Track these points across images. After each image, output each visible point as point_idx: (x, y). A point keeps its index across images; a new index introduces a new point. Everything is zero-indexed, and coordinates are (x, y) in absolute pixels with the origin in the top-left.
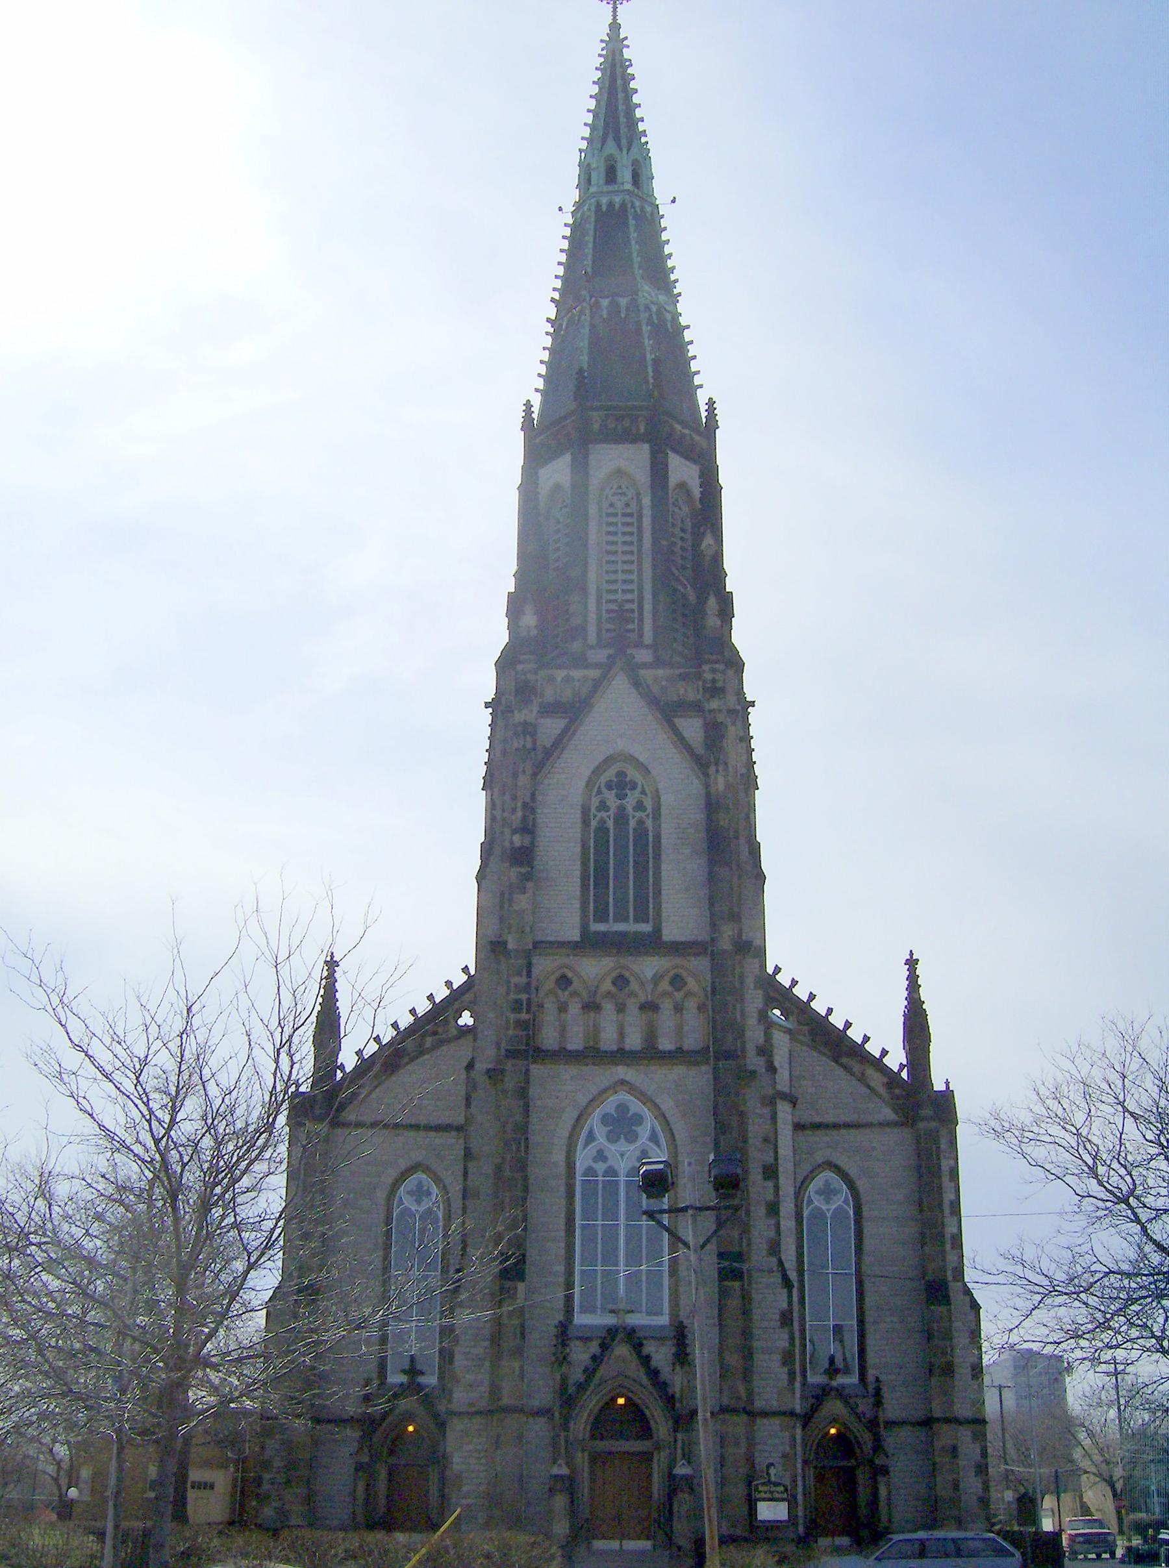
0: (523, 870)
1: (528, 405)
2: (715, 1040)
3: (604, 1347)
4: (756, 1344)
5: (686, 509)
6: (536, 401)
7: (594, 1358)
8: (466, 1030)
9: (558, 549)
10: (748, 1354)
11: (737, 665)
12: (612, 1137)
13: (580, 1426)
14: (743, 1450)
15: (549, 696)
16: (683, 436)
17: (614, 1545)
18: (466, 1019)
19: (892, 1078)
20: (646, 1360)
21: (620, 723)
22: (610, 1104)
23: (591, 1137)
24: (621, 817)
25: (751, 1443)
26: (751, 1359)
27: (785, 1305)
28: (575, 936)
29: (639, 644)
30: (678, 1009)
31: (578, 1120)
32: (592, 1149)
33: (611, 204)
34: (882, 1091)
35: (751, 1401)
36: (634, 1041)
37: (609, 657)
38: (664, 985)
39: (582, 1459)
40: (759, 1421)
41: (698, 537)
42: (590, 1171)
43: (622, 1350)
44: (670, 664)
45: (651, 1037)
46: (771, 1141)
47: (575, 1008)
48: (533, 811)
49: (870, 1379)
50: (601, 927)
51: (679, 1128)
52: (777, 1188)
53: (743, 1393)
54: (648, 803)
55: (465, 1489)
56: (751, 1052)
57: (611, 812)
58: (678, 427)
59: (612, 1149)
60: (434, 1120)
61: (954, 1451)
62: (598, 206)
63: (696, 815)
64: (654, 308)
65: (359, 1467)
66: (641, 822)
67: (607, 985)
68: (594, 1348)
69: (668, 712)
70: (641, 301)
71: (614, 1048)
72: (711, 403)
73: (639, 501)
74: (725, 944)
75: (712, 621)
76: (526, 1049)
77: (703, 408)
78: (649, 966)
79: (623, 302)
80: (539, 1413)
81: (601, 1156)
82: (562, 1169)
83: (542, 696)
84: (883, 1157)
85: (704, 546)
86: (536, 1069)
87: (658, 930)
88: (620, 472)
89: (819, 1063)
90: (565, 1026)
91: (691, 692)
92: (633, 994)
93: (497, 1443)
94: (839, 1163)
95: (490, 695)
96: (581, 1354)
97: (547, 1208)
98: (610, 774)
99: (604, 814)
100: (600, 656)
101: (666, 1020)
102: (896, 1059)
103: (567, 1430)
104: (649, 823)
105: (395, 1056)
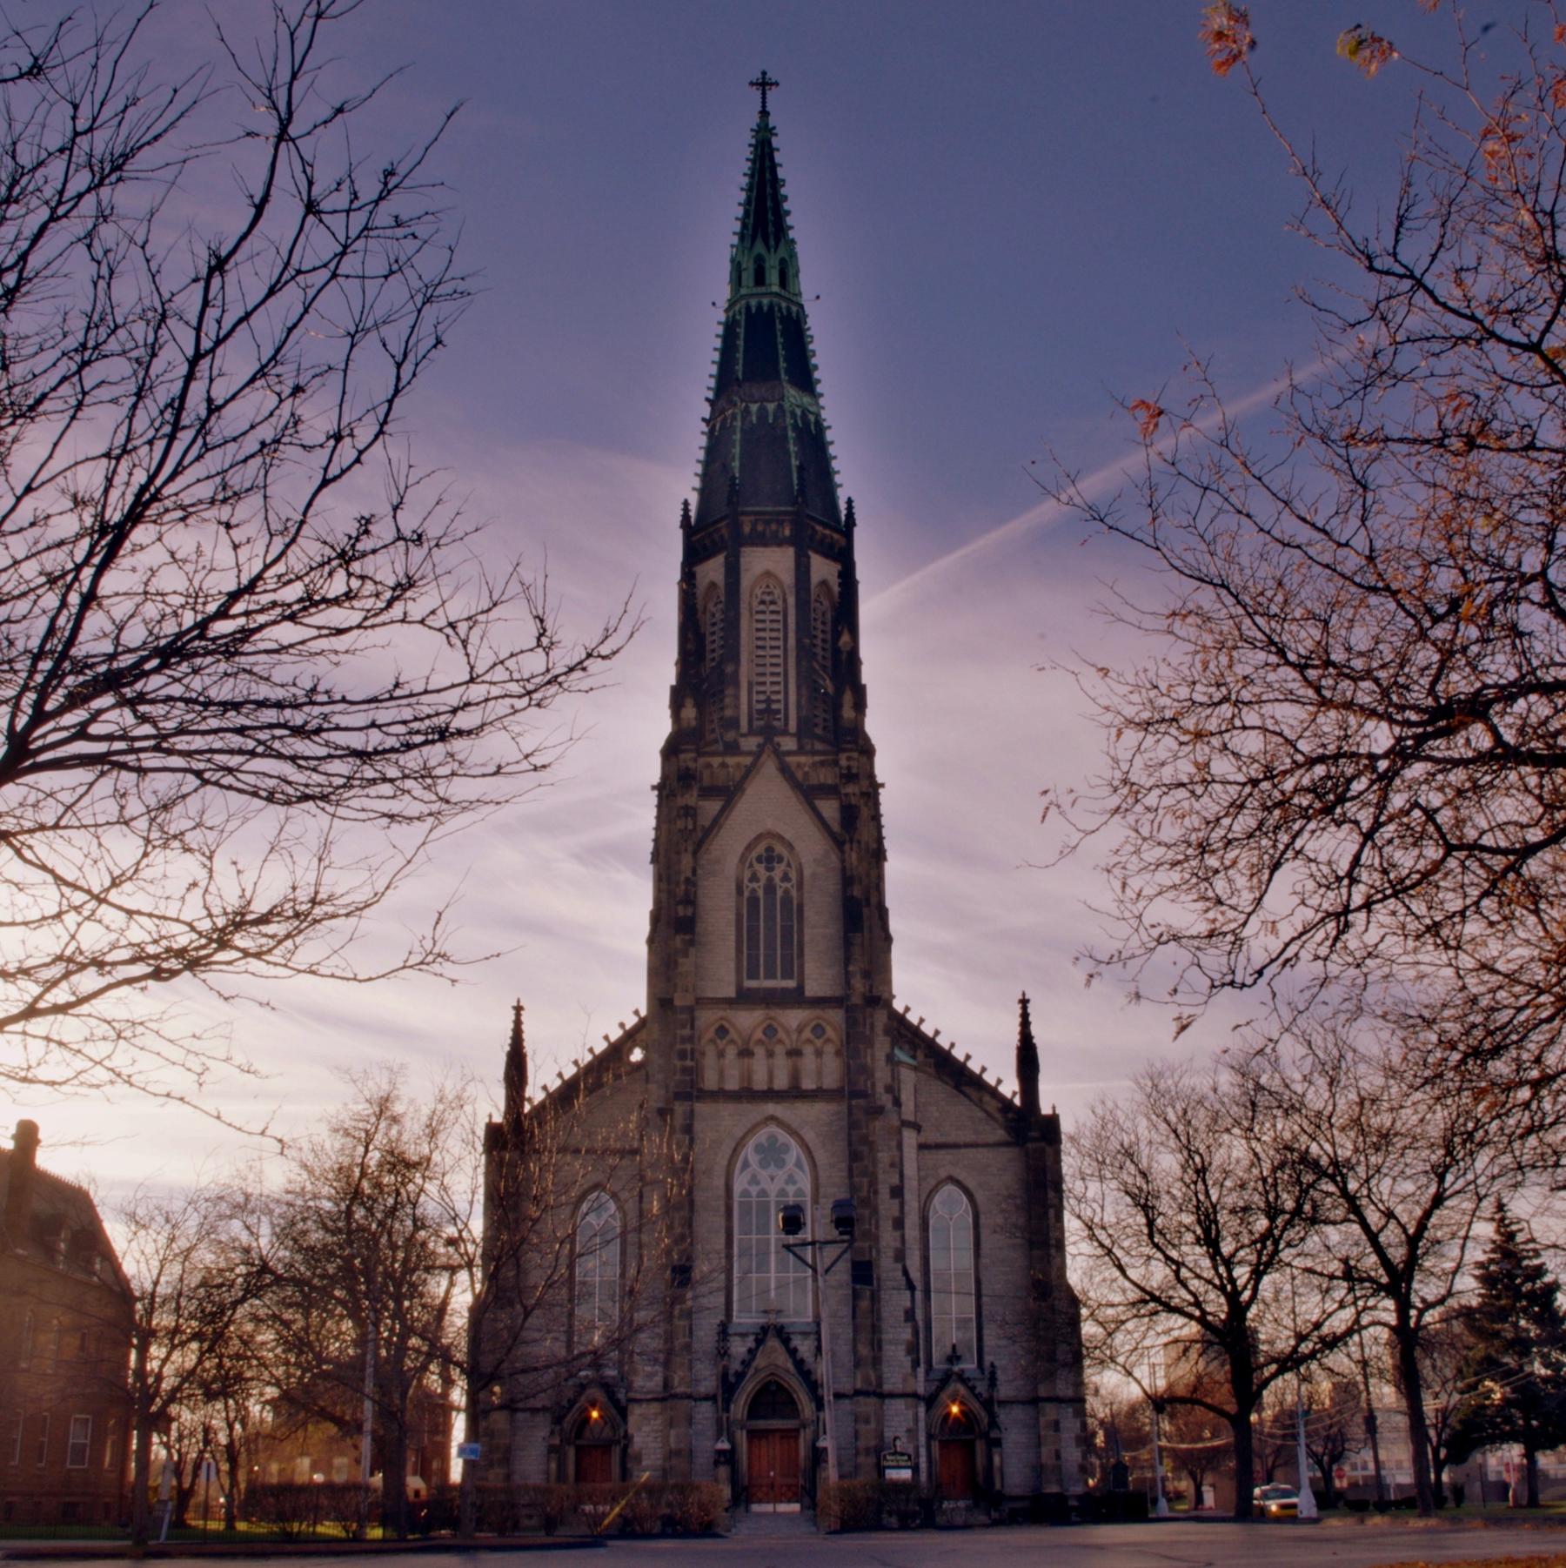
0: (687, 937)
1: (686, 503)
2: (850, 1082)
3: (759, 1341)
4: (884, 1336)
5: (826, 603)
6: (694, 499)
7: (750, 1351)
8: (639, 1066)
9: (714, 624)
10: (876, 1345)
11: (868, 751)
12: (764, 1164)
13: (739, 1408)
14: (873, 1425)
15: (706, 781)
16: (825, 536)
17: (769, 1508)
18: (637, 1055)
19: (1006, 1104)
20: (793, 1352)
21: (768, 807)
22: (762, 1136)
23: (746, 1165)
24: (770, 888)
25: (880, 1420)
26: (880, 1348)
27: (908, 1304)
28: (731, 992)
29: (785, 732)
30: (819, 1053)
31: (735, 1150)
32: (746, 1176)
33: (760, 306)
34: (998, 1115)
35: (880, 1384)
36: (781, 1082)
37: (759, 746)
38: (807, 1034)
39: (742, 1437)
40: (887, 1401)
41: (837, 635)
42: (746, 1193)
43: (773, 1343)
44: (814, 753)
45: (795, 1076)
46: (898, 1165)
47: (731, 1052)
48: (695, 885)
49: (987, 1364)
50: (752, 984)
51: (821, 1157)
52: (902, 1205)
53: (873, 1378)
54: (793, 875)
55: (644, 1463)
56: (880, 1089)
57: (762, 883)
58: (819, 528)
59: (764, 1174)
60: (315, 503)
61: (1056, 1426)
62: (748, 308)
63: (832, 885)
64: (798, 412)
65: (552, 1449)
66: (786, 891)
67: (759, 1034)
68: (750, 1342)
69: (809, 793)
70: (787, 406)
71: (765, 1088)
72: (850, 502)
73: (785, 601)
74: (856, 999)
75: (848, 713)
76: (690, 1091)
77: (843, 506)
78: (793, 1018)
79: (771, 407)
80: (706, 1398)
81: (754, 1180)
82: (722, 1192)
83: (701, 780)
84: (997, 1171)
85: (841, 643)
86: (700, 1108)
87: (800, 988)
88: (768, 574)
89: (938, 1090)
90: (722, 1070)
91: (826, 776)
92: (780, 1041)
93: (671, 1424)
94: (960, 1178)
95: (656, 779)
96: (739, 1348)
97: (709, 1226)
98: (760, 849)
99: (754, 885)
100: (750, 743)
101: (809, 1062)
102: (1010, 1087)
103: (728, 1410)
104: (794, 893)
105: (566, 1094)
